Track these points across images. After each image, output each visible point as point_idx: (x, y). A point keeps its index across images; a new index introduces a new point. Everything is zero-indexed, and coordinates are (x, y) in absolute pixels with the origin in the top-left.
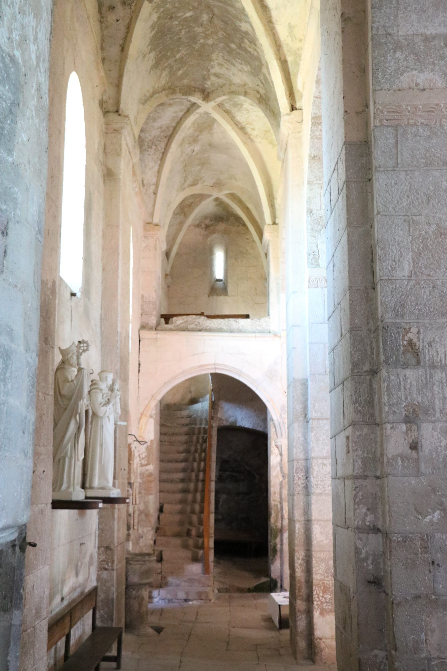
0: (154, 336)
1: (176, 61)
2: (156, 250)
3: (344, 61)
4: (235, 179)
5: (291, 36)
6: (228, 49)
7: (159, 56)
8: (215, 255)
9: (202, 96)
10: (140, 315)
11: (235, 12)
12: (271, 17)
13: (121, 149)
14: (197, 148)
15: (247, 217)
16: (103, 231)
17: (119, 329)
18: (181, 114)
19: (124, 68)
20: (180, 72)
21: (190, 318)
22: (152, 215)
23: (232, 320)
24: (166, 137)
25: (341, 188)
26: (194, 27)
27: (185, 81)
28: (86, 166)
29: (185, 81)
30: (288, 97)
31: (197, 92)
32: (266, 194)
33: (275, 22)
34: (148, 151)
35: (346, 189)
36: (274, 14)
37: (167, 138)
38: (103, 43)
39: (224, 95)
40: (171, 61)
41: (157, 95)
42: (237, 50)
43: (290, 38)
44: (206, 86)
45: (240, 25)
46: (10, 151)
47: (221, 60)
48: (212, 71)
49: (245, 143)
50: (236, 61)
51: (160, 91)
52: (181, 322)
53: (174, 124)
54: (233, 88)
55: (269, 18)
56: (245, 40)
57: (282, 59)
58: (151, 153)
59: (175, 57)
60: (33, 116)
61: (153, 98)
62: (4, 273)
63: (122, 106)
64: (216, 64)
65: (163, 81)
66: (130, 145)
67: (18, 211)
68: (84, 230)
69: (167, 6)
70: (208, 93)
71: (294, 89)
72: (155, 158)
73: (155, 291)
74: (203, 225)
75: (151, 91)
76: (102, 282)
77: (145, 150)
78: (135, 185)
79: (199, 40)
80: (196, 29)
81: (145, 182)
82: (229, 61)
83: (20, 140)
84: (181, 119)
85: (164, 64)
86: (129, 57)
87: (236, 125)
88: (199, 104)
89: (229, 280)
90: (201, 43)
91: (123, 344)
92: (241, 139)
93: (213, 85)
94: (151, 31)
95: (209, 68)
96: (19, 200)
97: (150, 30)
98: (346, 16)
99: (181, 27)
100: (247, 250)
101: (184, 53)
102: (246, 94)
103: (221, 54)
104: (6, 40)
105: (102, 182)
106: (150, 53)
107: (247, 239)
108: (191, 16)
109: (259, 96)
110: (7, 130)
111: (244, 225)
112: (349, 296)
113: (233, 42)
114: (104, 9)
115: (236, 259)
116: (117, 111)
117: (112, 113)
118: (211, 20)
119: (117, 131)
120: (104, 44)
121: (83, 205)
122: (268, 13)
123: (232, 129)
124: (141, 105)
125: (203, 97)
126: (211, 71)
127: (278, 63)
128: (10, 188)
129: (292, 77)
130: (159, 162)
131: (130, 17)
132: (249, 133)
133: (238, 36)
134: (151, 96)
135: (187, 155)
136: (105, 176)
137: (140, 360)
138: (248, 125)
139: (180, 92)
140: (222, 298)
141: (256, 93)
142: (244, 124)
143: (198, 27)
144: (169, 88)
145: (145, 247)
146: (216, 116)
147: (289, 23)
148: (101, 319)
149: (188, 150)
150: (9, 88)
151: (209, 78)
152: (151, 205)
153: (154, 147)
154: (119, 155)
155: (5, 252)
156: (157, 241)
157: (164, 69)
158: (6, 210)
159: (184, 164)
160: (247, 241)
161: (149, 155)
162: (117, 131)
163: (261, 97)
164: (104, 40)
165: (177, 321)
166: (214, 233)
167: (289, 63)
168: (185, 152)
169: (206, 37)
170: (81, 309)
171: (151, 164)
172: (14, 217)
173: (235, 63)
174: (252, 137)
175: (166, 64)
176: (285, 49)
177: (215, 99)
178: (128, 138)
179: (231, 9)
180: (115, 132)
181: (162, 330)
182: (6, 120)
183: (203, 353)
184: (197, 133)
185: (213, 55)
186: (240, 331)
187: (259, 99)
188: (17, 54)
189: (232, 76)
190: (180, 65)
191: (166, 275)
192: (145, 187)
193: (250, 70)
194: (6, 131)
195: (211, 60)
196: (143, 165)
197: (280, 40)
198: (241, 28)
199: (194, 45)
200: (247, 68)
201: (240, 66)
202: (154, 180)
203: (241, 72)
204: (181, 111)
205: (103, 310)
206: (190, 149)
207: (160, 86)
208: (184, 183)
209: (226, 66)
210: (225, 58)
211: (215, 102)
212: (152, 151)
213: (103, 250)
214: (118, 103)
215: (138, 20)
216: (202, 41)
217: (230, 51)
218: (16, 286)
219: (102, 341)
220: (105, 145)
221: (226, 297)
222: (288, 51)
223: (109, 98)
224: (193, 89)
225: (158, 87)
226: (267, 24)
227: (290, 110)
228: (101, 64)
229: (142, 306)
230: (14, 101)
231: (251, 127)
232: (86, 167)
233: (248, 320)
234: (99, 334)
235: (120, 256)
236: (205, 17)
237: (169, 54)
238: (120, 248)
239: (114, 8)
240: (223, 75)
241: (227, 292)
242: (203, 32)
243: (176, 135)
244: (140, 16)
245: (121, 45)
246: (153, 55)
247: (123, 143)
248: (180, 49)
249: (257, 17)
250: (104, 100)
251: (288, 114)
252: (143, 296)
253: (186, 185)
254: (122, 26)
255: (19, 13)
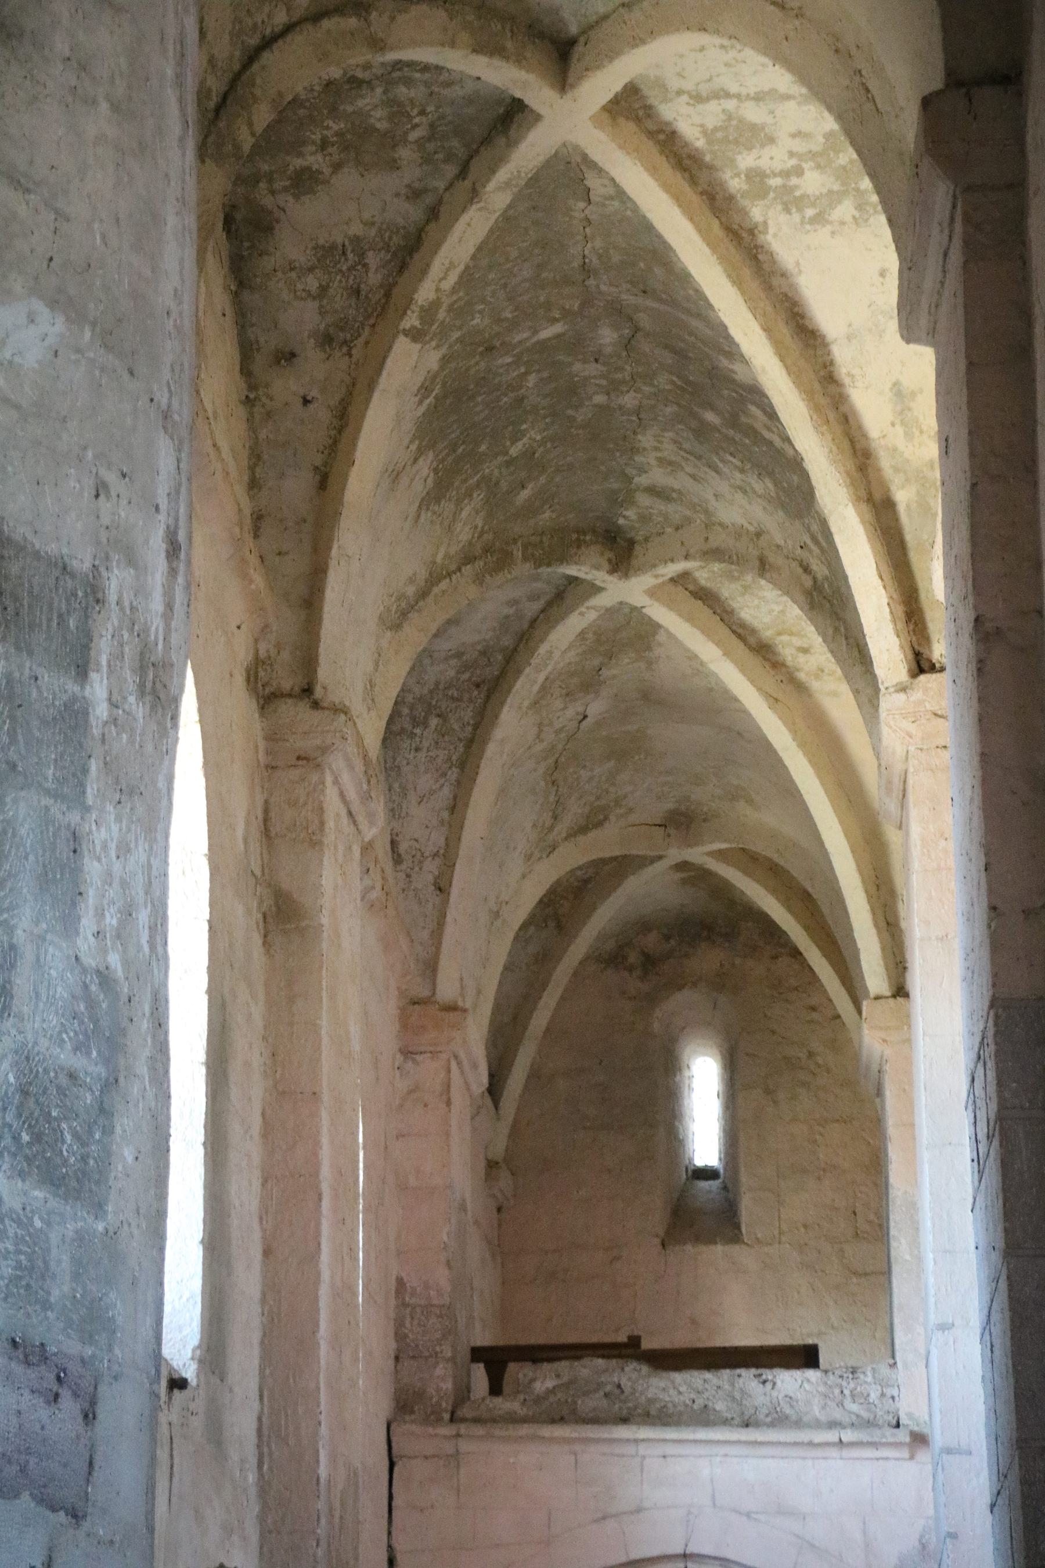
0: (449, 1448)
1: (508, 464)
2: (448, 1103)
3: (986, 759)
4: (750, 801)
5: (902, 423)
6: (694, 424)
7: (450, 459)
8: (686, 1073)
9: (609, 555)
10: (391, 1362)
11: (709, 332)
12: (832, 363)
13: (322, 823)
14: (596, 708)
15: (806, 928)
16: (263, 1114)
17: (323, 1471)
18: (532, 608)
19: (330, 549)
20: (525, 494)
21: (588, 1368)
22: (431, 968)
23: (747, 1378)
24: (478, 686)
25: (991, 1134)
26: (571, 364)
27: (547, 516)
28: (209, 922)
29: (547, 516)
30: (901, 625)
31: (588, 545)
32: (864, 882)
33: (847, 381)
34: (412, 735)
35: (1001, 1142)
36: (843, 355)
37: (485, 688)
38: (255, 465)
39: (687, 557)
40: (491, 468)
41: (444, 584)
42: (724, 430)
43: (899, 430)
44: (621, 521)
45: (731, 367)
46: (98, 1208)
47: (669, 450)
48: (643, 480)
49: (773, 701)
50: (723, 461)
51: (453, 567)
52: (550, 1384)
53: (507, 641)
54: (719, 539)
55: (825, 367)
56: (753, 409)
57: (877, 496)
58: (426, 744)
59: (506, 453)
60: (145, 1089)
61: (430, 599)
62: (89, 1518)
63: (323, 673)
64: (653, 462)
65: (464, 534)
66: (352, 794)
67: (117, 1351)
68: (204, 1144)
69: (475, 322)
70: (631, 543)
71: (923, 595)
72: (439, 761)
73: (448, 1263)
74: (633, 958)
75: (423, 574)
76: (264, 1300)
77: (403, 730)
78: (368, 882)
79: (590, 398)
80: (577, 367)
81: (403, 847)
82: (699, 458)
83: (120, 1168)
84: (533, 622)
85: (465, 481)
86: (344, 512)
87: (740, 637)
88: (598, 583)
89: (744, 1178)
90: (596, 406)
91: (337, 1514)
92: (759, 689)
93: (644, 519)
94: (420, 402)
95: (629, 471)
96: (119, 1320)
97: (417, 399)
98: (989, 626)
99: (523, 370)
100: (811, 1055)
101: (538, 438)
102: (763, 567)
103: (669, 434)
104: (92, 939)
105: (260, 942)
106: (416, 460)
107: (813, 1009)
108: (558, 336)
109: (808, 582)
110: (95, 1159)
111: (796, 953)
112: (1020, 1466)
113: (712, 407)
114: (259, 363)
115: (768, 1091)
116: (307, 691)
117: (290, 701)
118: (628, 344)
119: (307, 759)
120: (258, 470)
121: (202, 1056)
122: (819, 352)
123: (725, 654)
124: (388, 634)
125: (610, 561)
126: (636, 480)
127: (860, 515)
128: (101, 1299)
129: (914, 557)
130: (453, 774)
131: (348, 379)
132: (789, 663)
133: (726, 392)
134: (423, 594)
135: (558, 732)
136: (270, 920)
137: (394, 1542)
138: (785, 638)
139: (525, 559)
140: (719, 1249)
141: (800, 570)
142: (767, 634)
143: (585, 361)
144: (487, 550)
145: (410, 1092)
146: (659, 613)
147: (896, 384)
148: (259, 1431)
149: (565, 715)
150: (99, 1052)
151: (629, 500)
152: (425, 934)
153: (434, 722)
154: (315, 843)
155: (91, 1464)
156: (454, 1065)
157: (469, 495)
158: (93, 1356)
159: (551, 761)
160: (815, 1015)
161: (417, 750)
162: (307, 759)
163: (816, 586)
164: (259, 457)
165: (533, 1380)
166: (680, 988)
167: (901, 508)
168: (551, 724)
169: (614, 388)
170: (197, 1423)
171: (426, 782)
172: (109, 1368)
173: (721, 465)
174: (802, 676)
175: (473, 481)
176: (885, 463)
177: (654, 566)
178: (346, 778)
179: (695, 323)
180: (300, 763)
181: (477, 1420)
182: (91, 1133)
183: (639, 1510)
184: (596, 662)
185: (639, 437)
186: (779, 1420)
187: (808, 594)
188: (114, 960)
189: (712, 498)
190: (523, 474)
191: (492, 1165)
192: (404, 866)
193: (773, 494)
194: (92, 1162)
195: (634, 450)
196: (396, 785)
197: (865, 436)
198: (736, 377)
199: (570, 412)
200: (763, 486)
201: (738, 475)
202: (437, 839)
203: (745, 492)
204: (533, 597)
205: (266, 1399)
206: (570, 712)
207: (453, 551)
208: (551, 829)
209: (689, 469)
210: (687, 446)
211: (656, 576)
212: (428, 736)
213: (265, 1182)
214: (309, 661)
215: (376, 396)
216: (600, 399)
217: (702, 431)
218: (112, 1542)
219: (262, 1519)
220: (266, 811)
221: (735, 1249)
222: (897, 470)
223: (279, 646)
224: (575, 536)
225: (447, 556)
226: (817, 386)
227: (909, 671)
228: (249, 538)
229: (399, 1323)
230: (107, 1079)
231: (797, 642)
232: (210, 928)
233: (811, 1374)
234: (253, 1492)
235: (326, 1204)
236: (607, 336)
237: (483, 448)
238: (326, 1171)
239: (293, 355)
240: (680, 492)
241: (738, 1227)
242: (602, 376)
243: (515, 680)
244: (383, 381)
245: (316, 468)
246: (425, 466)
247: (331, 798)
248: (524, 426)
249: (784, 372)
250: (262, 654)
251: (903, 689)
252: (400, 1282)
253: (562, 828)
254: (322, 413)
255: (118, 857)
